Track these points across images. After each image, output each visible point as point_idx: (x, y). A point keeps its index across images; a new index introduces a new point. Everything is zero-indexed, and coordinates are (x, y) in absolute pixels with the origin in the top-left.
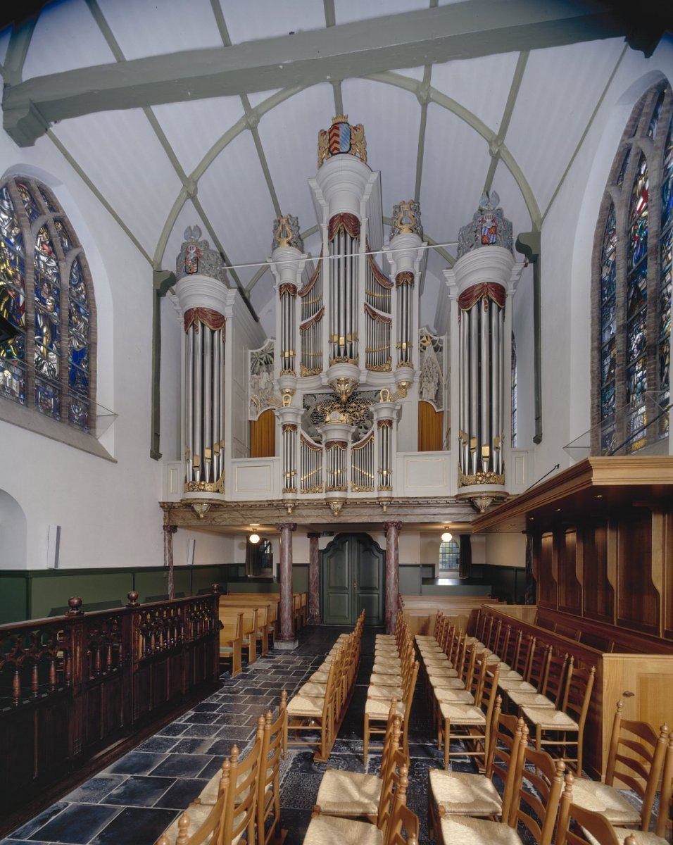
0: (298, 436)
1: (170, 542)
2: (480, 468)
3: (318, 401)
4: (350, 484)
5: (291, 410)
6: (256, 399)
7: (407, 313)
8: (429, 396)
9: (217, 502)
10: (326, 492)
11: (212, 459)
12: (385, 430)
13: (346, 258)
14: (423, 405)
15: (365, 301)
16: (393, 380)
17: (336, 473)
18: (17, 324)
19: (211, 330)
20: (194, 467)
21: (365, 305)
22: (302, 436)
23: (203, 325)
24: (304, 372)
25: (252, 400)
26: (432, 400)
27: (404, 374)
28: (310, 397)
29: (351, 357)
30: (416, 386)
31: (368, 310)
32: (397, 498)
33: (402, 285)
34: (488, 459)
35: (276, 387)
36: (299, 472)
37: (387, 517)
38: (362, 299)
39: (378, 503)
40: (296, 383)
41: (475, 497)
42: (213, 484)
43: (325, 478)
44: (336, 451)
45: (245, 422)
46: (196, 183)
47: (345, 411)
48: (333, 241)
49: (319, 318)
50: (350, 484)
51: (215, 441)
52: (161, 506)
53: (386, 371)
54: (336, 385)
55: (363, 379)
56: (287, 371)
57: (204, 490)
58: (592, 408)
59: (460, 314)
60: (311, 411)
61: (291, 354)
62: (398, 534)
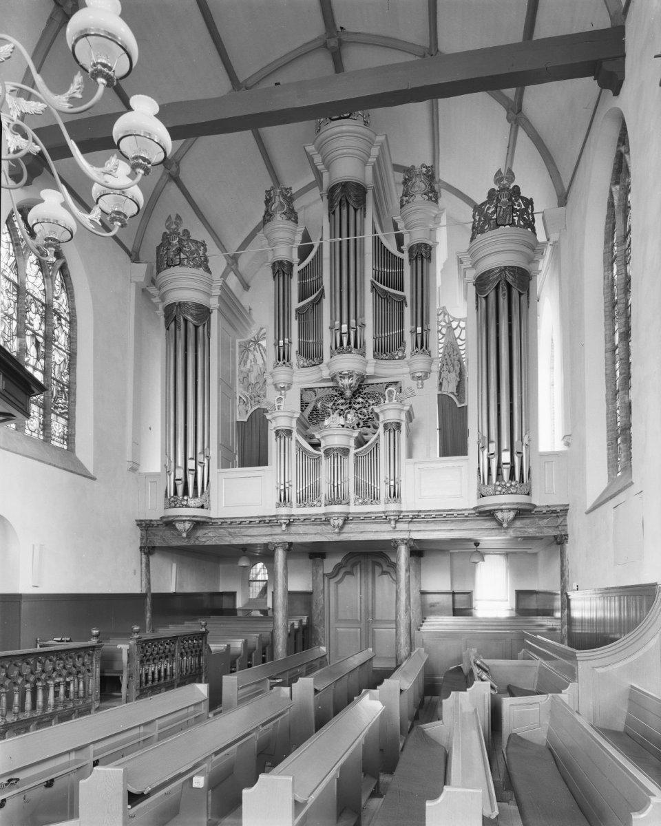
0: (294, 442)
1: (148, 565)
2: (499, 474)
3: (318, 397)
4: (352, 496)
5: (282, 414)
8: (449, 388)
9: (202, 519)
10: (326, 505)
11: (196, 470)
13: (348, 240)
14: (443, 400)
16: (407, 370)
17: (336, 484)
18: (27, 364)
19: (195, 325)
20: (175, 480)
21: (372, 282)
22: (297, 441)
23: (186, 321)
24: (301, 362)
25: (240, 398)
26: (452, 393)
27: (420, 363)
28: (309, 392)
29: (356, 346)
30: (434, 378)
31: (374, 287)
33: (416, 258)
35: (270, 381)
36: (294, 483)
38: (369, 276)
39: (385, 518)
40: (292, 376)
41: (495, 510)
42: (197, 500)
43: (325, 489)
45: (233, 423)
46: (178, 164)
47: (350, 408)
48: (334, 213)
49: (318, 301)
50: (352, 496)
51: (199, 449)
52: (138, 525)
53: (399, 359)
54: (338, 379)
55: (370, 370)
56: (281, 362)
57: (187, 506)
58: (607, 414)
59: (477, 300)
60: (309, 409)
61: (286, 342)
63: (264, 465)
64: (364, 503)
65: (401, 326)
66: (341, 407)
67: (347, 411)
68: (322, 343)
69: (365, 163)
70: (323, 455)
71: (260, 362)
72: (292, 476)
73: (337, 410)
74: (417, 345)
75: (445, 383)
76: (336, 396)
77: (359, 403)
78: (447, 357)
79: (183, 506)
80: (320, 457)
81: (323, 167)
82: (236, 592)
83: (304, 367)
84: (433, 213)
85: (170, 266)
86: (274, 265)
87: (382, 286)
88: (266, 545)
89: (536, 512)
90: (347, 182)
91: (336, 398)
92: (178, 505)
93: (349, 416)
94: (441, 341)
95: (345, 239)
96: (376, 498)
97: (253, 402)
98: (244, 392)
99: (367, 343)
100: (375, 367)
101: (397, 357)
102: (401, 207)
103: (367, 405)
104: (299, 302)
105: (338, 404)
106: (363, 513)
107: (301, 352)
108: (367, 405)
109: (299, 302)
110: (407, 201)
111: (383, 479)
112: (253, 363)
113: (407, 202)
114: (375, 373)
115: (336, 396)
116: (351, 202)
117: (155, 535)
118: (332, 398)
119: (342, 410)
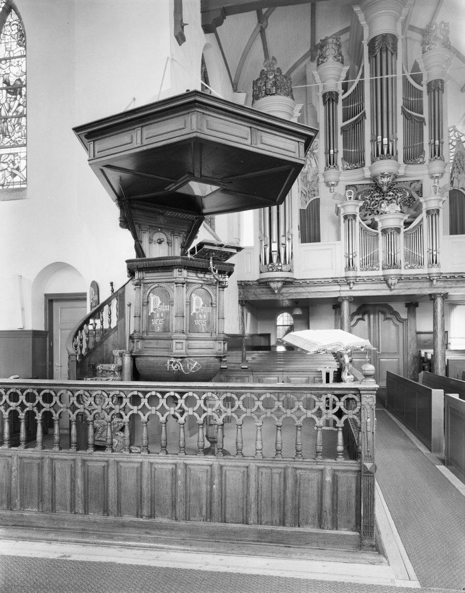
0: (357, 224)
3: (359, 191)
6: (305, 191)
7: (434, 112)
12: (434, 218)
13: (381, 75)
15: (402, 105)
16: (427, 171)
21: (402, 107)
22: (360, 223)
24: (346, 166)
25: (302, 192)
31: (404, 112)
32: (446, 273)
34: (276, 253)
35: (322, 180)
36: (358, 254)
37: (434, 289)
40: (339, 176)
44: (392, 236)
47: (383, 199)
49: (360, 122)
53: (420, 163)
55: (401, 172)
57: (281, 270)
62: (134, 445)
63: (318, 242)
64: (412, 268)
65: (421, 139)
66: (376, 199)
67: (381, 201)
68: (364, 151)
69: (396, 19)
70: (380, 233)
71: (314, 165)
72: (357, 247)
73: (373, 200)
74: (330, 163)
75: (455, 181)
76: (372, 190)
77: (390, 196)
78: (457, 162)
79: (278, 270)
80: (377, 234)
81: (365, 22)
82: (46, 295)
83: (347, 169)
84: (446, 57)
85: (268, 95)
86: (324, 96)
87: (409, 111)
88: (337, 298)
89: (443, 277)
90: (386, 34)
91: (372, 192)
92: (275, 270)
93: (383, 205)
94: (451, 151)
95: (385, 77)
96: (421, 264)
97: (310, 195)
98: (304, 188)
99: (398, 153)
100: (405, 169)
101: (419, 163)
102: (423, 53)
103: (396, 197)
104: (343, 121)
105: (374, 197)
106: (413, 275)
107: (346, 158)
108: (396, 197)
109: (343, 121)
110: (322, 61)
111: (426, 250)
112: (310, 166)
113: (322, 62)
114: (405, 174)
115: (372, 190)
116: (390, 48)
117: (248, 292)
118: (370, 192)
119: (377, 201)
